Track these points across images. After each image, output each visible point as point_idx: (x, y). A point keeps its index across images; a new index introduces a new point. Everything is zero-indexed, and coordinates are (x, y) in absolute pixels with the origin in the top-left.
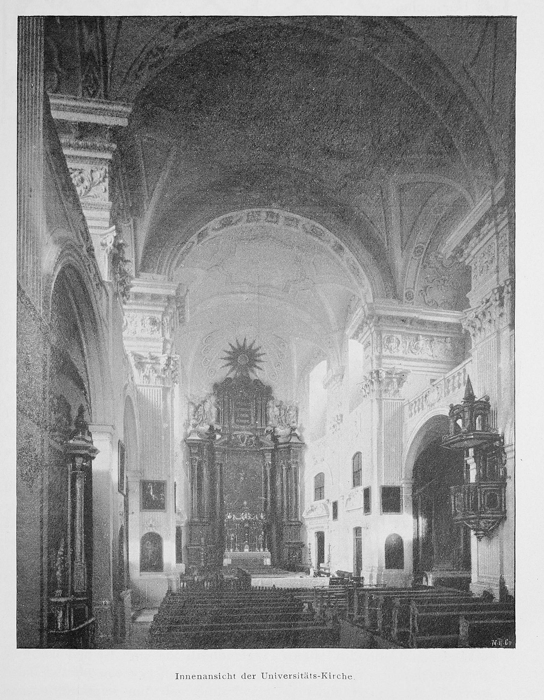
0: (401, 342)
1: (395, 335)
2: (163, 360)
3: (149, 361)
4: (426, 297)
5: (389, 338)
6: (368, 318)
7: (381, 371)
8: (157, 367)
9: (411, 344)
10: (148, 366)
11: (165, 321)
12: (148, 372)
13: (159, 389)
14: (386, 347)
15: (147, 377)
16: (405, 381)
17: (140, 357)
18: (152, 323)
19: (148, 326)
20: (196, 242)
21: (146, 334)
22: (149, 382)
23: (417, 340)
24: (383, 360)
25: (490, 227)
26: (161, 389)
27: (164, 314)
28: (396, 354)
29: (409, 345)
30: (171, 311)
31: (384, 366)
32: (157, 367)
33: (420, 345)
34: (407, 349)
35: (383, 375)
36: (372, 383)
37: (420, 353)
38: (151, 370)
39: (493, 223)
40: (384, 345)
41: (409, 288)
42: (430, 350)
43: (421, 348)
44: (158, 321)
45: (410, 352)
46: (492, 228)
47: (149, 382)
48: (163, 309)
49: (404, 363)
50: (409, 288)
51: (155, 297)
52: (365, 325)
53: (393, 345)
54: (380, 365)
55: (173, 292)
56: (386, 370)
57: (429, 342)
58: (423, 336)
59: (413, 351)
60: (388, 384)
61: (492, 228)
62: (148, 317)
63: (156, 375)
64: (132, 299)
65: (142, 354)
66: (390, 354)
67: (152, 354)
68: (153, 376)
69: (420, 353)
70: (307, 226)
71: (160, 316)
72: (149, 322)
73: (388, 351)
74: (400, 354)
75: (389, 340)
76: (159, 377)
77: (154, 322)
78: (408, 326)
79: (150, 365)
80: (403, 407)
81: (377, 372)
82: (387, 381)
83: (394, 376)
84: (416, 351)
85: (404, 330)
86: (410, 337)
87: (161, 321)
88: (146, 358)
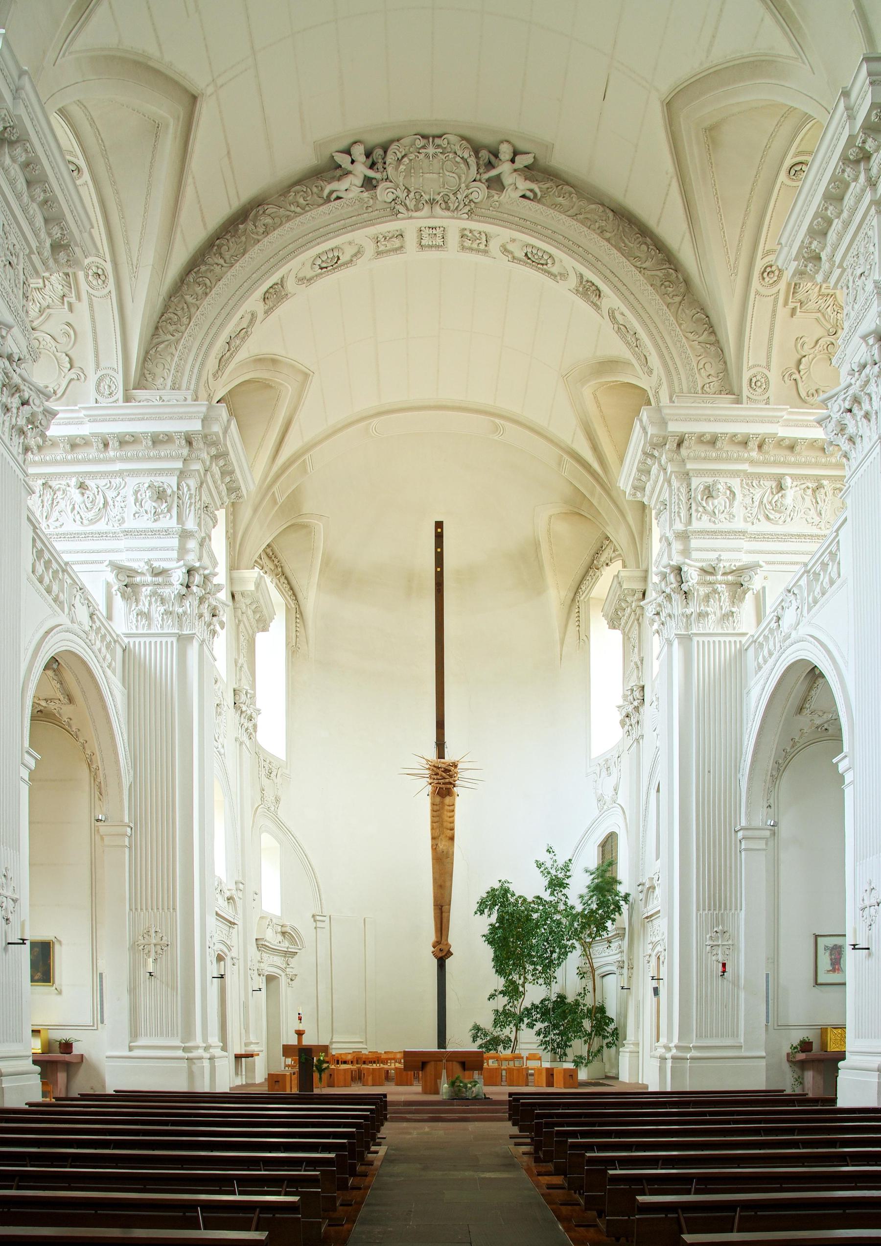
0: (739, 496)
1: (722, 480)
2: (178, 576)
3: (149, 578)
4: (800, 385)
5: (707, 488)
6: (654, 446)
7: (685, 569)
8: (166, 591)
9: (765, 501)
10: (145, 591)
11: (186, 489)
12: (147, 604)
13: (169, 640)
14: (700, 509)
15: (147, 616)
16: (748, 589)
17: (131, 573)
18: (155, 497)
19: (149, 505)
20: (260, 315)
21: (145, 523)
22: (149, 625)
23: (780, 488)
24: (694, 543)
25: (858, 189)
26: (175, 640)
27: (182, 474)
28: (725, 526)
29: (761, 502)
30: (197, 466)
31: (695, 555)
32: (166, 591)
33: (789, 501)
34: (755, 511)
35: (692, 576)
36: (669, 597)
37: (789, 519)
38: (153, 599)
39: (862, 178)
40: (697, 506)
41: (754, 366)
42: (813, 510)
43: (790, 508)
44: (169, 492)
45: (761, 517)
46: (863, 191)
47: (149, 625)
48: (179, 465)
49: (746, 545)
50: (754, 366)
51: (157, 440)
52: (649, 461)
53: (720, 501)
54: (686, 552)
55: (196, 426)
56: (699, 564)
57: (809, 492)
58: (794, 477)
59: (771, 517)
60: (707, 597)
61: (863, 191)
62: (9, 398)
63: (162, 609)
64: (114, 450)
65: (135, 565)
66: (711, 526)
67: (156, 564)
68: (157, 610)
69: (789, 519)
70: (510, 247)
71: (173, 481)
72: (149, 494)
73: (705, 518)
74: (739, 524)
75: (709, 492)
76: (167, 612)
77: (160, 495)
78: (754, 454)
79: (150, 588)
80: (742, 652)
81: (679, 570)
82: (703, 591)
83: (719, 578)
84: (777, 515)
85: (745, 467)
86: (762, 482)
87: (175, 489)
88: (142, 574)
